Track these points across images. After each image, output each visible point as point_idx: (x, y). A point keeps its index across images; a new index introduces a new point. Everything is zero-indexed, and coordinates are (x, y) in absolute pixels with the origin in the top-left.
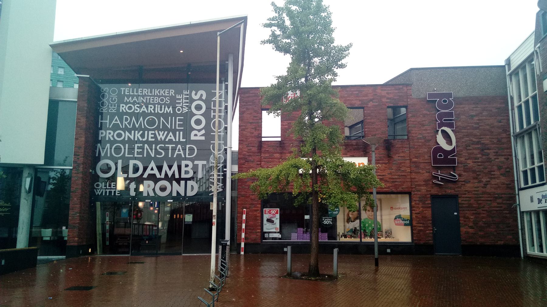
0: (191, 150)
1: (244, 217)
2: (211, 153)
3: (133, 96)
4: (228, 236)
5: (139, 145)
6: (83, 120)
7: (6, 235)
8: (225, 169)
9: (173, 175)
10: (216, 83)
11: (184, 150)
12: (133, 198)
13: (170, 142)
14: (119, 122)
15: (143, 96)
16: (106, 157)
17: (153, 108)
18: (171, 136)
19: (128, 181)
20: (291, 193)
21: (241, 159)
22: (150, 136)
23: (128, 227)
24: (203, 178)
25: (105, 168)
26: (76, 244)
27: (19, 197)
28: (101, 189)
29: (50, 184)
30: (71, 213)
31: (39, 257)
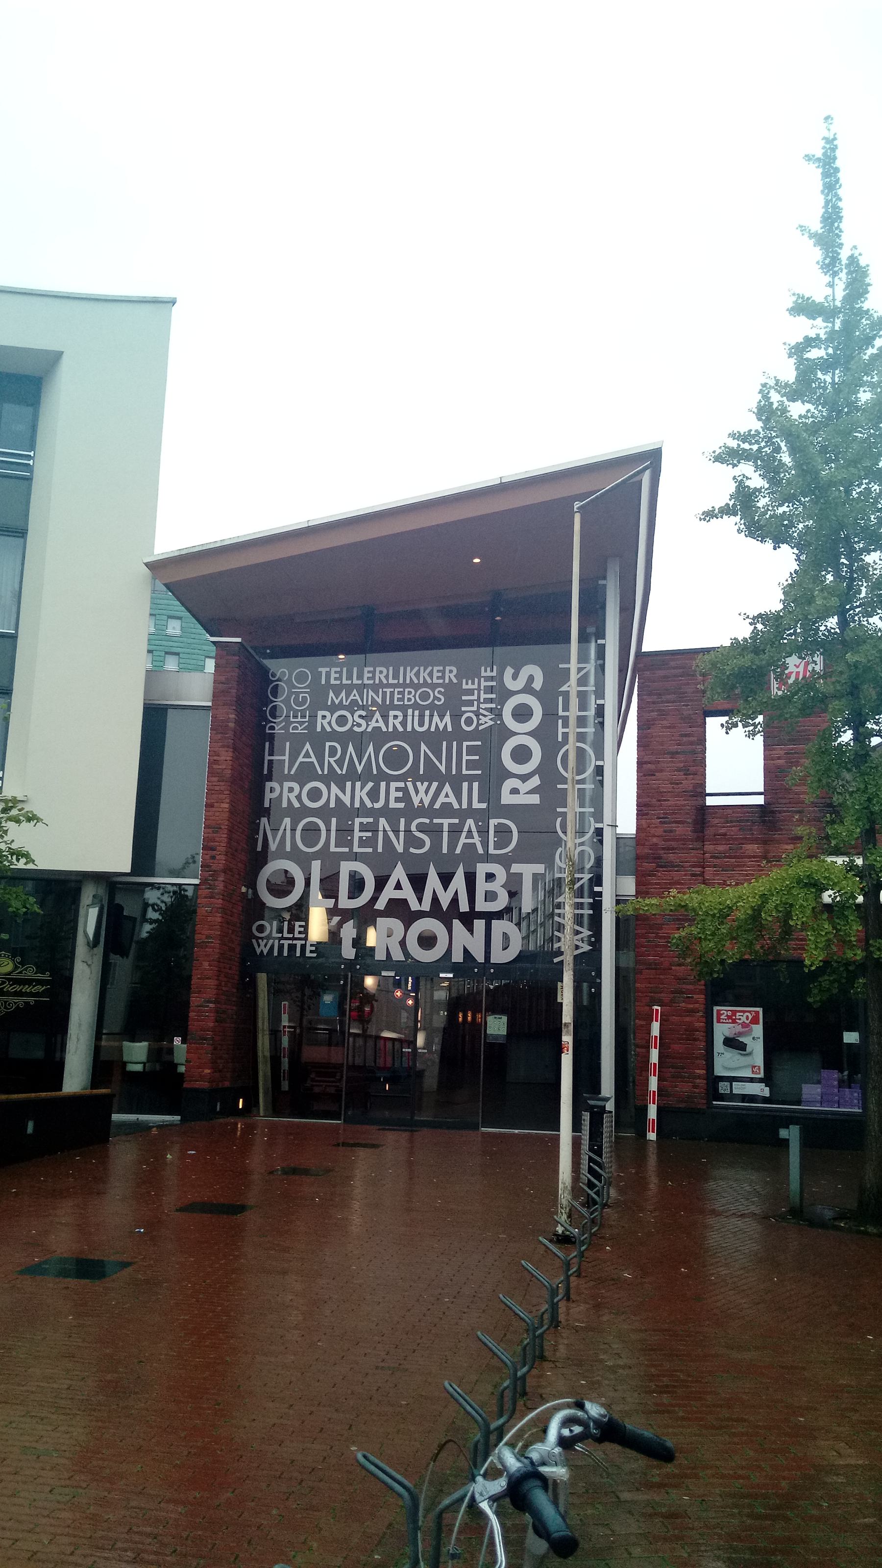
0: (503, 833)
1: (656, 1029)
2: (559, 842)
3: (349, 689)
4: (608, 1087)
5: (365, 820)
6: (226, 756)
7: (40, 1054)
8: (596, 889)
9: (455, 901)
10: (568, 640)
11: (483, 832)
12: (350, 964)
13: (447, 810)
14: (313, 759)
15: (375, 688)
16: (281, 854)
17: (400, 719)
18: (447, 796)
19: (336, 919)
20: (800, 962)
21: (646, 857)
22: (393, 794)
23: (337, 1045)
24: (535, 910)
25: (280, 880)
26: (205, 1085)
27: (71, 956)
28: (270, 938)
29: (144, 920)
30: (195, 1000)
31: (115, 1117)
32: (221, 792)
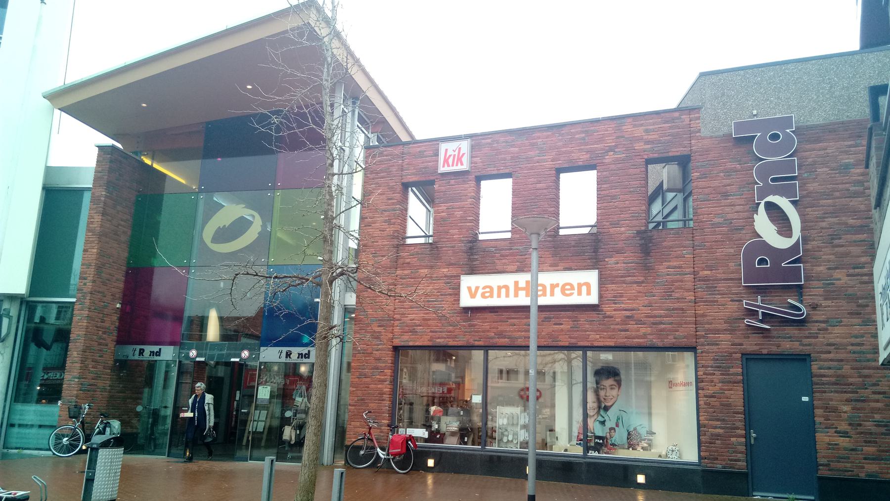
32: (92, 242)
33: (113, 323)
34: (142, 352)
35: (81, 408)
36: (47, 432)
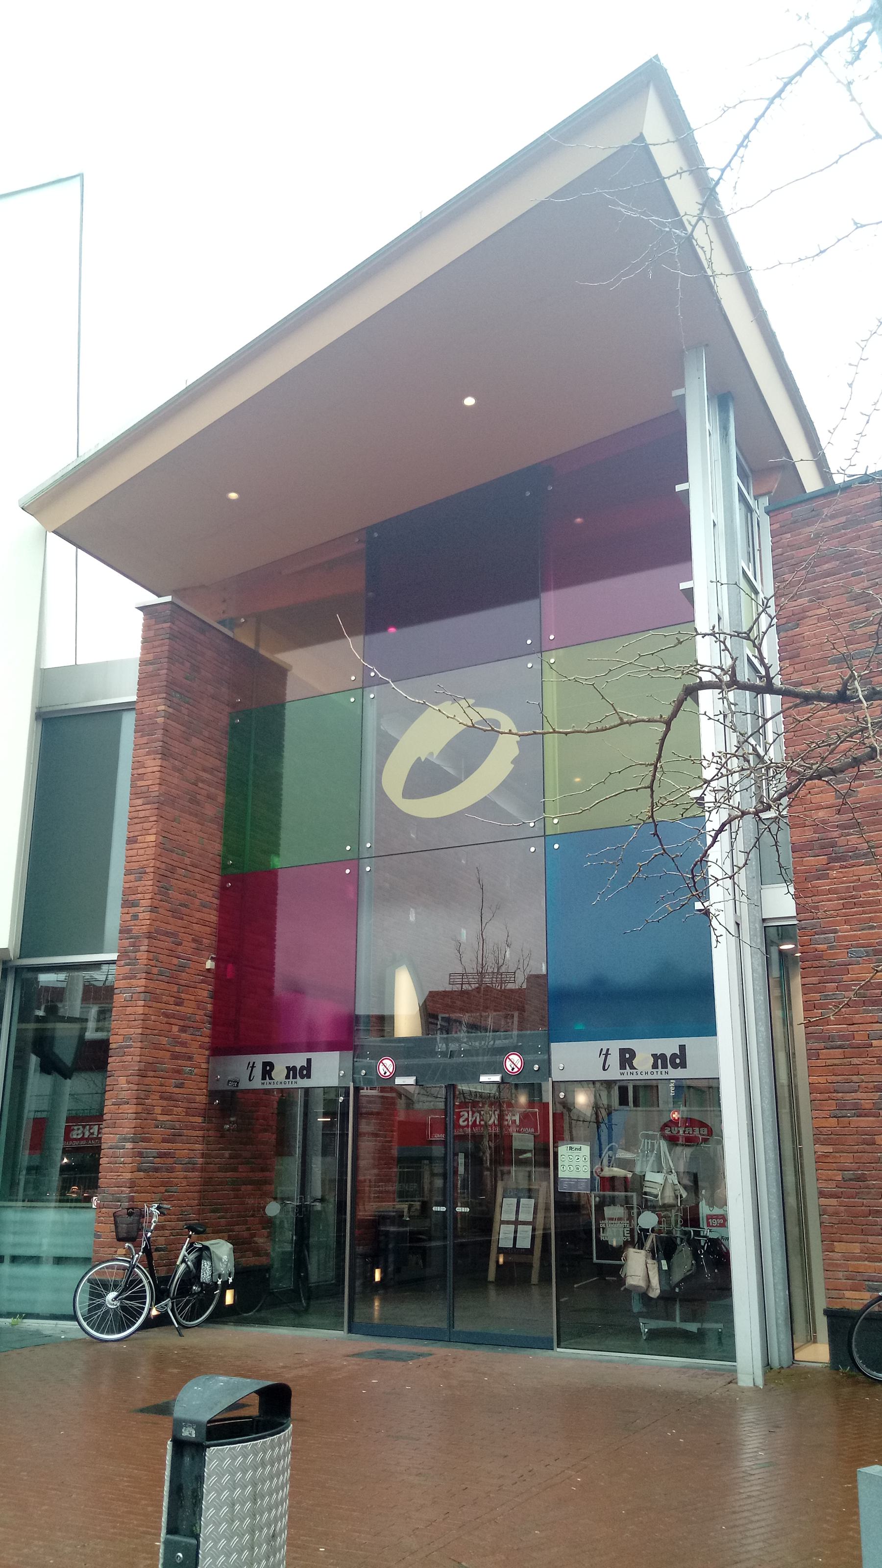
33: (199, 1004)
34: (268, 1070)
35: (142, 1215)
36: (73, 1273)
